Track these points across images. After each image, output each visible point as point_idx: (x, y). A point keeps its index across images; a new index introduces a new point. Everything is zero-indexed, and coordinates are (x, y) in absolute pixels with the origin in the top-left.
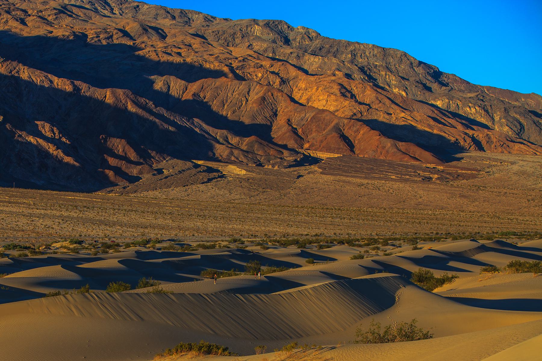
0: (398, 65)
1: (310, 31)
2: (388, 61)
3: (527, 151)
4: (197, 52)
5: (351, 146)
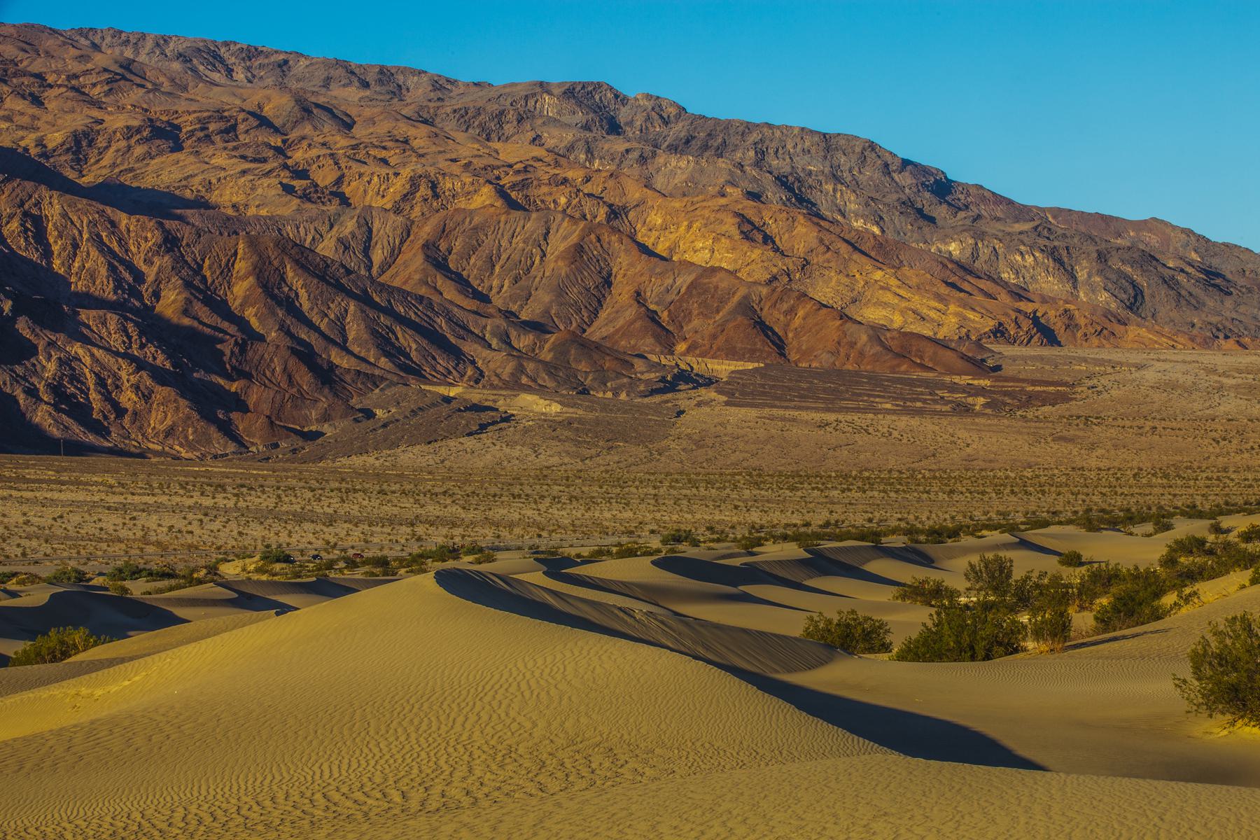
0: (857, 169)
1: (664, 104)
2: (835, 163)
3: (1156, 342)
4: (422, 156)
5: (780, 345)
